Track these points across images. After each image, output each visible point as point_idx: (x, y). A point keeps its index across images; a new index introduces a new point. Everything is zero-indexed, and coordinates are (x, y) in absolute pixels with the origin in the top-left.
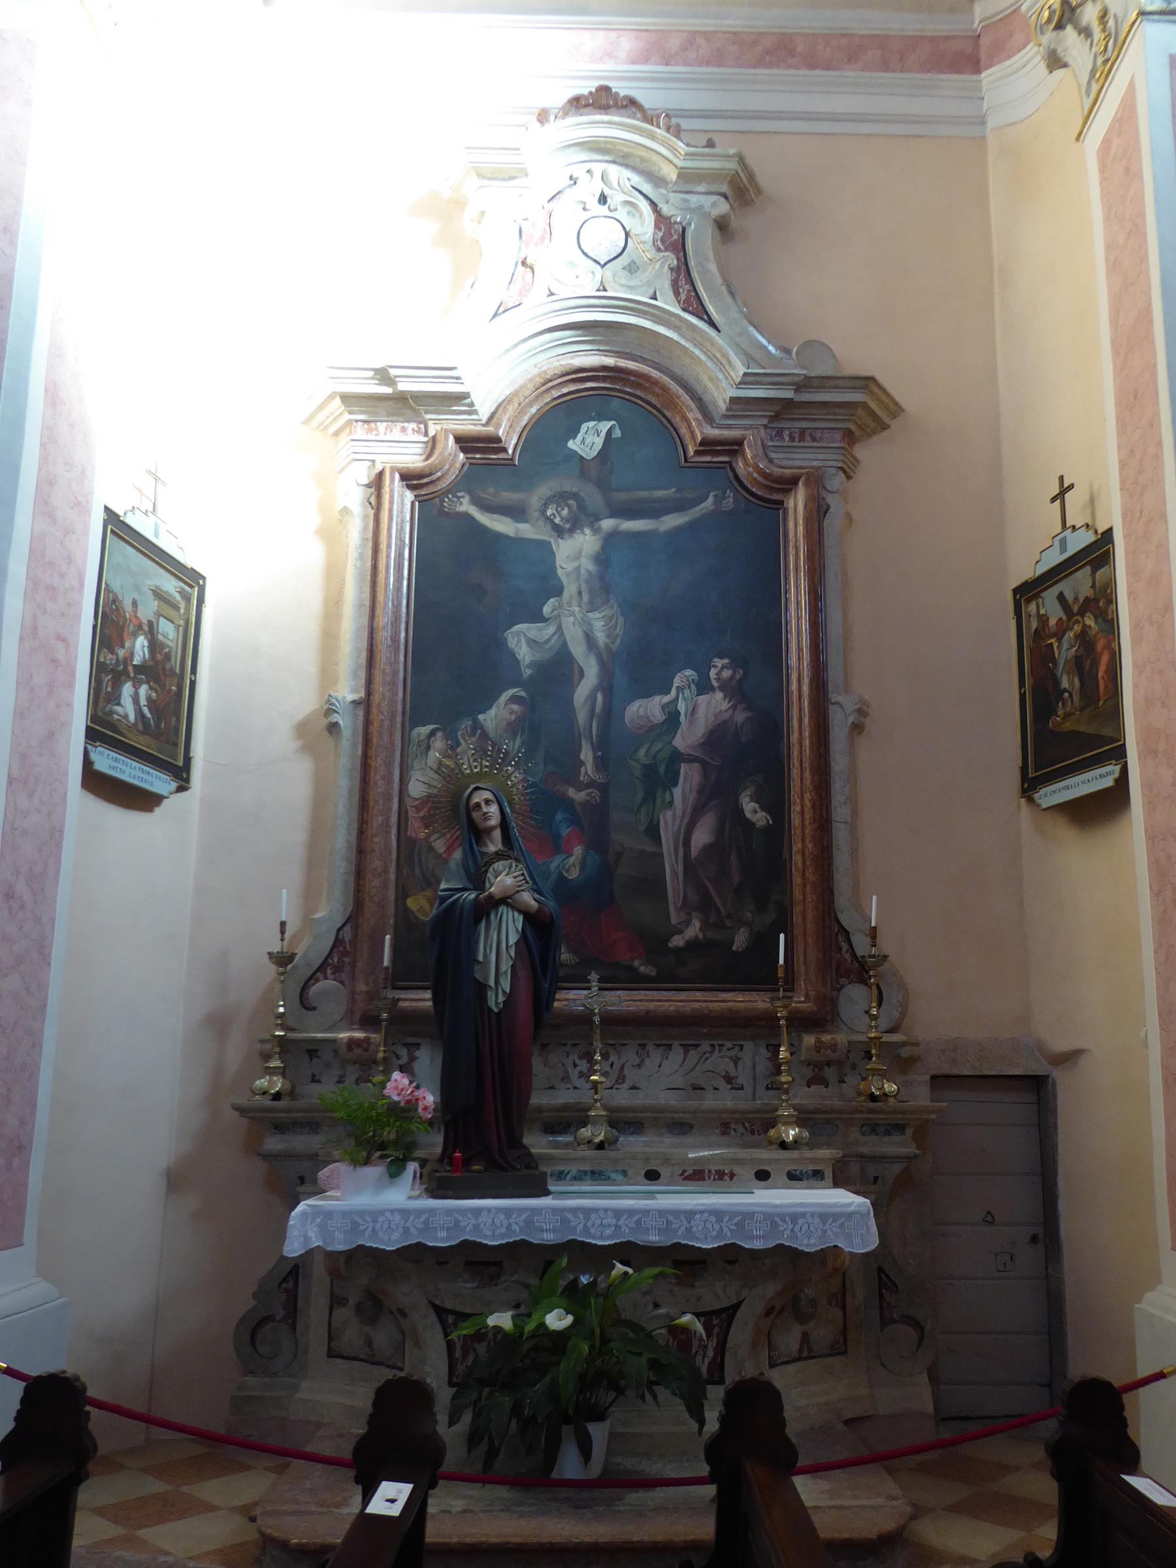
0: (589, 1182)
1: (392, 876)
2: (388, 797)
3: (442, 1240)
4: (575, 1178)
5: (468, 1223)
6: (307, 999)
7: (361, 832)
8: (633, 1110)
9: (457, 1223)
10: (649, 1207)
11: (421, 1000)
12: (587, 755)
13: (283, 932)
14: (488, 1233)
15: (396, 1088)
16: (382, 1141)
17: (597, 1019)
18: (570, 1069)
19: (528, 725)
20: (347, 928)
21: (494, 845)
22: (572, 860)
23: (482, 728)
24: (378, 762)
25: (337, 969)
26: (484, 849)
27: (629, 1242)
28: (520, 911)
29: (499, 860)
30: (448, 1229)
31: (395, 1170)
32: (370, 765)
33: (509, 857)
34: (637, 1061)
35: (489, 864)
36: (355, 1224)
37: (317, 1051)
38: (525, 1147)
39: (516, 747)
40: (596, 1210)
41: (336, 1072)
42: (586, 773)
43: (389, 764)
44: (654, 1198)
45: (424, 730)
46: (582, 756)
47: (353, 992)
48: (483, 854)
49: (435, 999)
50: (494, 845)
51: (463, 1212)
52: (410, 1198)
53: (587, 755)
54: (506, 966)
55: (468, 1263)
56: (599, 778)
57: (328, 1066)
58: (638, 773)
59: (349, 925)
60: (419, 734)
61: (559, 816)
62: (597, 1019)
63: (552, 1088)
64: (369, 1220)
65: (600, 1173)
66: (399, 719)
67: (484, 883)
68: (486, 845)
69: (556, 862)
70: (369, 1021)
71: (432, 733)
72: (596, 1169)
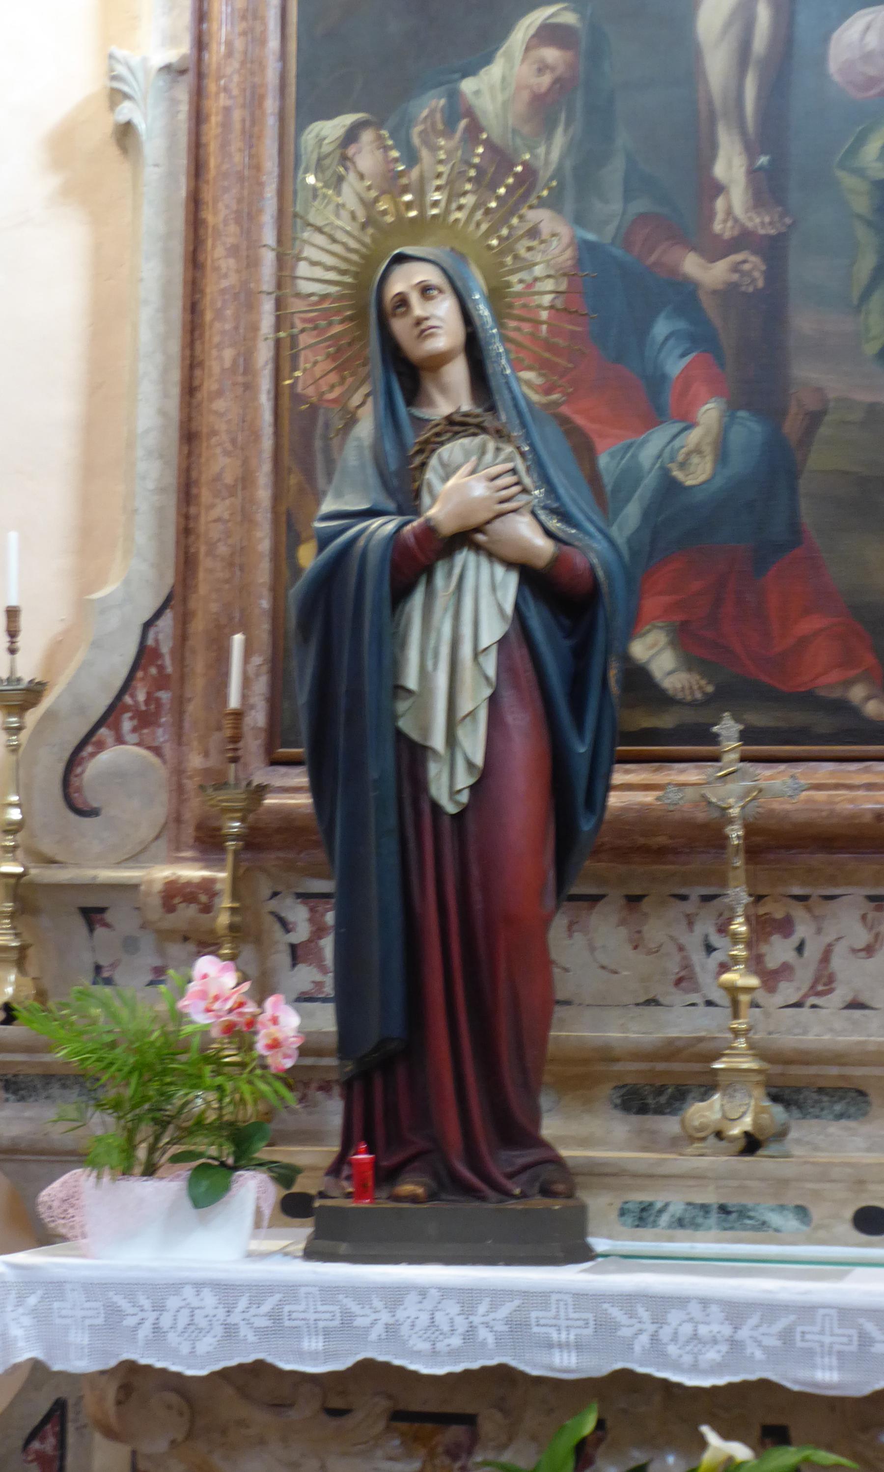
0: (714, 1232)
1: (264, 494)
2: (247, 300)
3: (314, 1356)
4: (680, 1223)
5: (373, 1319)
6: (79, 790)
7: (190, 389)
8: (838, 1058)
9: (347, 1317)
10: (815, 1298)
11: (290, 793)
12: (730, 166)
13: (13, 633)
14: (425, 1346)
15: (203, 995)
16: (178, 1122)
17: (735, 833)
18: (697, 957)
19: (579, 97)
20: (167, 622)
21: (452, 394)
22: (694, 436)
23: (470, 113)
24: (220, 213)
25: (146, 719)
26: (423, 413)
27: (764, 1384)
28: (509, 564)
29: (456, 435)
30: (327, 1333)
31: (209, 1186)
32: (204, 222)
33: (481, 429)
34: (862, 937)
35: (428, 447)
36: (114, 1313)
37: (102, 910)
38: (542, 1144)
39: (555, 155)
40: (680, 1301)
41: (148, 959)
42: (729, 212)
43: (247, 217)
44: (840, 1277)
45: (331, 129)
46: (720, 170)
47: (179, 771)
48: (419, 423)
49: (317, 788)
50: (452, 394)
51: (362, 1293)
52: (251, 1255)
53: (730, 166)
54: (474, 698)
55: (398, 1416)
56: (761, 223)
57: (130, 945)
58: (862, 204)
59: (168, 615)
60: (320, 141)
61: (661, 328)
62: (735, 833)
63: (652, 1002)
64: (146, 1303)
65: (743, 1213)
66: (271, 105)
67: (417, 494)
68: (431, 403)
69: (653, 446)
70: (208, 842)
71: (351, 136)
72: (732, 1201)
